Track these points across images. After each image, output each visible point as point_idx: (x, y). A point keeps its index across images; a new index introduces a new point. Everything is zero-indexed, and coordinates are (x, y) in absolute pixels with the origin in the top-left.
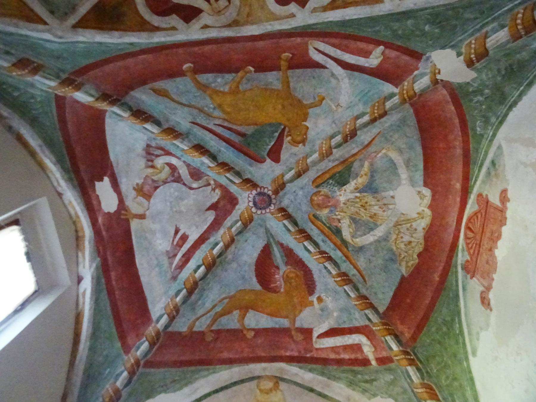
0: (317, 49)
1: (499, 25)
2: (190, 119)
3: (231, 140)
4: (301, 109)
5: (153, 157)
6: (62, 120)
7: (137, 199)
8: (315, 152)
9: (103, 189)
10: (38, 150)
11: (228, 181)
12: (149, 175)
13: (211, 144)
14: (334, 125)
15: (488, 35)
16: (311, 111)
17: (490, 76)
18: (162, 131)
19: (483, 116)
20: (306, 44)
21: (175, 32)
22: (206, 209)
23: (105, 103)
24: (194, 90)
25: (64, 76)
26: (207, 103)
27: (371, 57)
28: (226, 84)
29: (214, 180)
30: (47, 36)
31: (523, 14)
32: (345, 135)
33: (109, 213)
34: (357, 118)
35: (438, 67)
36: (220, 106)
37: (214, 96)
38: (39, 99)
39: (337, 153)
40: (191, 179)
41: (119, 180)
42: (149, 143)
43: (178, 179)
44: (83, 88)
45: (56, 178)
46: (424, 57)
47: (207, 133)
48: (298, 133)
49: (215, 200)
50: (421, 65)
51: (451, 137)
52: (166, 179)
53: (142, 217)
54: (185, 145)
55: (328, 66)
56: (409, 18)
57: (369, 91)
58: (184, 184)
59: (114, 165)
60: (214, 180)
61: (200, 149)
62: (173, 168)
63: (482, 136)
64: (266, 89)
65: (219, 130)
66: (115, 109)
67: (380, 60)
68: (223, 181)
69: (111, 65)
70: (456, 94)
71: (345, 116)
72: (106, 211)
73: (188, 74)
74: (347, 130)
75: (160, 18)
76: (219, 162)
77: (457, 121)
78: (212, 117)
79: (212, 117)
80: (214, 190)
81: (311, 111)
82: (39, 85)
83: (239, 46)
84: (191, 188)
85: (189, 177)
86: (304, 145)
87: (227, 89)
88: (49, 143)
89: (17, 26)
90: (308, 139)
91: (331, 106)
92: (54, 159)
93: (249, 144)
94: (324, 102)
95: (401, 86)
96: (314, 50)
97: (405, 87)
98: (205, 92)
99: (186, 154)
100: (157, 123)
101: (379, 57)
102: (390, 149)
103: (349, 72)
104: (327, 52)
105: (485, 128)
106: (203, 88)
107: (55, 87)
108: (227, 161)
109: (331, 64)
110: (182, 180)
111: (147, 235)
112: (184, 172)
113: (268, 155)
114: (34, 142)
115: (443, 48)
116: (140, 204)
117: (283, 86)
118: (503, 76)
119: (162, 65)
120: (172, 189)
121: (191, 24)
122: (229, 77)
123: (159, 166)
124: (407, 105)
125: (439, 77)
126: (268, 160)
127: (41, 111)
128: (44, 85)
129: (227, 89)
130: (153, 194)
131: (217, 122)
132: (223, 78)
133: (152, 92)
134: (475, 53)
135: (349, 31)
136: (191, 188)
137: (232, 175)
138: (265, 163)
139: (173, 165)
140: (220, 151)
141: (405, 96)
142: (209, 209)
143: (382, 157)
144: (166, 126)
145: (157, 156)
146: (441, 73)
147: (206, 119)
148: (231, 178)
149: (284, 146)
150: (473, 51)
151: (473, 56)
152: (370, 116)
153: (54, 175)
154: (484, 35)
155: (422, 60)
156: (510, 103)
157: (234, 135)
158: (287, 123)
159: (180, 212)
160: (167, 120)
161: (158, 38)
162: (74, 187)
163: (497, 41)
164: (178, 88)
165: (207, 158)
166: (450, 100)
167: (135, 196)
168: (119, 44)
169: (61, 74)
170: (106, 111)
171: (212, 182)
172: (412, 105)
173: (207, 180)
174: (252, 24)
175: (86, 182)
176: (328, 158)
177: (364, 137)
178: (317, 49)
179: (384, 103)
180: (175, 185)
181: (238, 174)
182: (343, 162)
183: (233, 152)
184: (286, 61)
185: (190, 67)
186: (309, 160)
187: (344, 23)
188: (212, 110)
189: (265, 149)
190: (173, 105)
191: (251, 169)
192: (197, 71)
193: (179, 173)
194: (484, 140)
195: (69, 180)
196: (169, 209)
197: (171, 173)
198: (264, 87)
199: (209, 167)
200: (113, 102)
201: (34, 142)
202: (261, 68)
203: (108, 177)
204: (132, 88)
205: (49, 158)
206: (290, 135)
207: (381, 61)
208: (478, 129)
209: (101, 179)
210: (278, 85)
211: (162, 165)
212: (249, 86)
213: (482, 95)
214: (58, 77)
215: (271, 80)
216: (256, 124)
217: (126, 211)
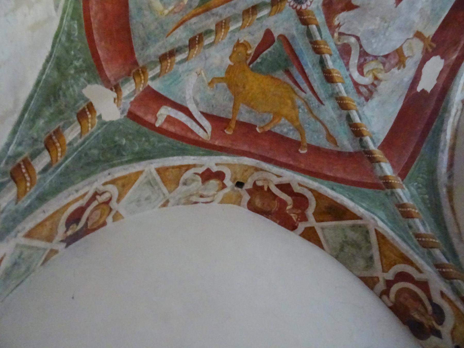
0: (204, 130)
1: (73, 145)
2: (323, 107)
3: (299, 72)
4: (231, 79)
5: (370, 87)
6: (412, 158)
7: (411, 55)
8: (232, 31)
9: (428, 83)
10: (447, 149)
11: (322, 30)
12: (383, 72)
13: (317, 75)
14: (207, 55)
15: (79, 136)
16: (223, 75)
17: (71, 89)
18: (349, 110)
19: (72, 41)
20: (212, 138)
21: (301, 183)
22: (359, 9)
23: (375, 156)
24: (307, 130)
25: (389, 191)
26: (302, 114)
27: (165, 116)
28: (281, 125)
29: (333, 36)
30: (380, 223)
31: (57, 156)
32: (200, 45)
33: (442, 58)
34: (186, 60)
35: (115, 105)
36: (294, 107)
37: (295, 118)
38: (416, 184)
39: (211, 23)
40: (352, 49)
41: (411, 82)
42: (365, 103)
43: (363, 54)
44: (383, 175)
45: (454, 120)
46: (126, 114)
47: (316, 89)
48: (240, 54)
49: (344, 15)
50: (128, 107)
51: (100, 16)
52: (372, 60)
53: (419, 35)
54: (339, 88)
55: (199, 113)
56: (137, 153)
57: (171, 84)
58: (361, 46)
59: (403, 97)
60: (333, 36)
61: (328, 77)
62: (360, 69)
63: (73, 19)
64: (252, 107)
65: (304, 86)
66: (372, 147)
67: (159, 113)
68: (326, 32)
69: (353, 179)
70: (97, 72)
71: (195, 63)
72: (443, 61)
73: (305, 144)
74: (197, 49)
75: (305, 194)
76: (319, 56)
77: (96, 37)
78: (305, 101)
79: (305, 101)
80: (339, 26)
81: (223, 75)
82: (409, 194)
83: (260, 152)
84: (358, 39)
85: (353, 52)
86: (238, 41)
87: (283, 120)
88: (435, 148)
89: (393, 239)
90: (233, 46)
91: (205, 75)
92: (442, 135)
93: (286, 60)
94: (210, 81)
95: (145, 87)
96: (207, 131)
97: (142, 85)
98: (300, 125)
99: (342, 78)
100: (349, 118)
101: (159, 115)
102: (159, 13)
103: (184, 104)
104: (198, 127)
105: (70, 27)
106: (299, 129)
107: (400, 188)
108: (311, 52)
109: (197, 115)
110: (360, 52)
111: (429, 12)
112: (354, 60)
113: (274, 41)
114: (444, 158)
115: (112, 123)
116: (410, 48)
117: (239, 105)
118: (60, 89)
119: (321, 161)
120: (374, 47)
121: (288, 182)
122: (277, 130)
123: (371, 76)
124: (141, 63)
125: (115, 95)
126: (276, 35)
127: (421, 175)
128: (404, 193)
129: (283, 120)
130: (393, 52)
131: (303, 94)
132: (282, 131)
133: (338, 144)
134: (87, 118)
135: (180, 144)
136: (358, 39)
137: (315, 36)
138: (279, 34)
139: (359, 71)
140: (314, 65)
141: (143, 78)
142: (357, 7)
143: (170, 4)
144: (345, 112)
145: (365, 86)
146: (113, 100)
147: (310, 101)
148: (317, 33)
149: (256, 45)
150: (90, 120)
151: (90, 116)
152: (175, 60)
153: (453, 123)
154: (83, 135)
155: (127, 111)
156: (52, 59)
157: (295, 75)
158: (246, 68)
159: (383, 19)
160: (340, 116)
161: (314, 184)
162: (448, 102)
163: (72, 130)
164: (318, 137)
165: (328, 66)
166: (103, 63)
167: (408, 59)
168: (340, 193)
169: (389, 193)
170: (379, 148)
171: (336, 35)
172: (136, 63)
173: (339, 39)
174: (246, 165)
175: (435, 98)
176: (221, 20)
177: (182, 36)
178: (204, 130)
179: (161, 71)
180: (369, 51)
181: (309, 34)
182: (208, 9)
183: (303, 59)
184: (230, 127)
185: (301, 150)
186: (240, 24)
187: (183, 152)
188: (302, 107)
189: (274, 49)
190: (328, 126)
191: (295, 33)
192: (298, 144)
193: (359, 60)
194: (70, 14)
195: (446, 110)
196: (389, 29)
197: (365, 64)
198: (253, 110)
199: (331, 55)
200: (369, 153)
201: (444, 158)
202: (250, 127)
203: (416, 89)
204: (351, 155)
205: (445, 138)
206: (247, 54)
207: (158, 111)
208: (76, 26)
209: (423, 91)
210: (243, 108)
211: (367, 75)
212: (265, 115)
213: (76, 68)
214: (393, 193)
215: (247, 115)
216: (272, 78)
217: (427, 50)
